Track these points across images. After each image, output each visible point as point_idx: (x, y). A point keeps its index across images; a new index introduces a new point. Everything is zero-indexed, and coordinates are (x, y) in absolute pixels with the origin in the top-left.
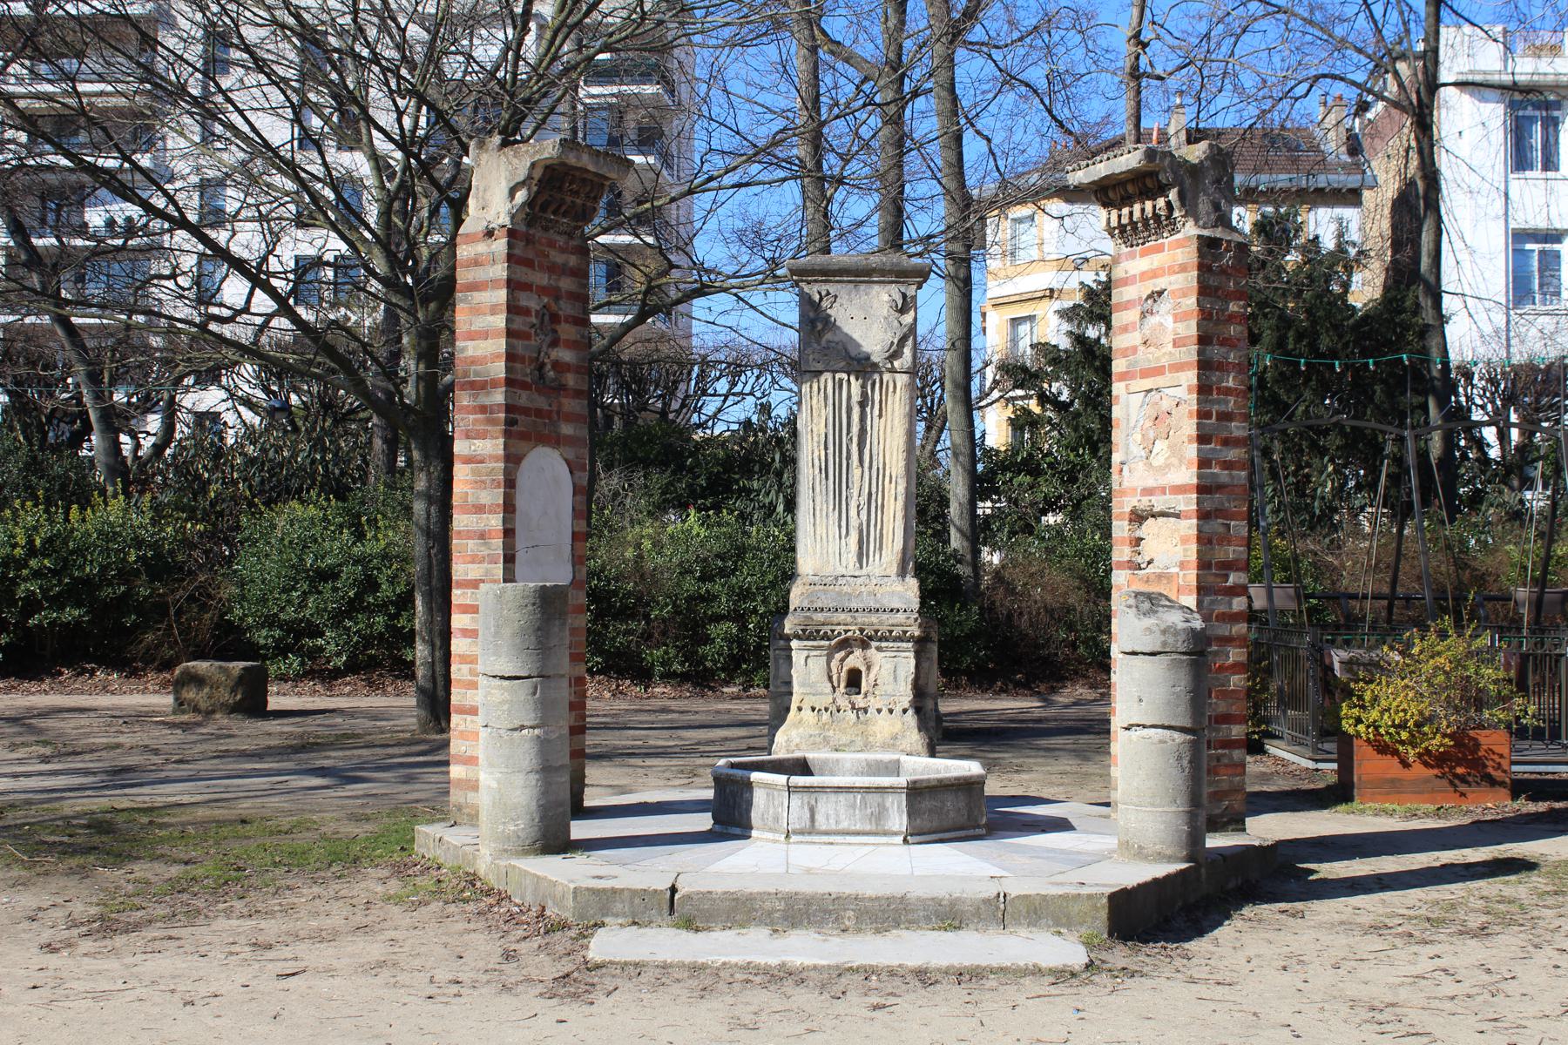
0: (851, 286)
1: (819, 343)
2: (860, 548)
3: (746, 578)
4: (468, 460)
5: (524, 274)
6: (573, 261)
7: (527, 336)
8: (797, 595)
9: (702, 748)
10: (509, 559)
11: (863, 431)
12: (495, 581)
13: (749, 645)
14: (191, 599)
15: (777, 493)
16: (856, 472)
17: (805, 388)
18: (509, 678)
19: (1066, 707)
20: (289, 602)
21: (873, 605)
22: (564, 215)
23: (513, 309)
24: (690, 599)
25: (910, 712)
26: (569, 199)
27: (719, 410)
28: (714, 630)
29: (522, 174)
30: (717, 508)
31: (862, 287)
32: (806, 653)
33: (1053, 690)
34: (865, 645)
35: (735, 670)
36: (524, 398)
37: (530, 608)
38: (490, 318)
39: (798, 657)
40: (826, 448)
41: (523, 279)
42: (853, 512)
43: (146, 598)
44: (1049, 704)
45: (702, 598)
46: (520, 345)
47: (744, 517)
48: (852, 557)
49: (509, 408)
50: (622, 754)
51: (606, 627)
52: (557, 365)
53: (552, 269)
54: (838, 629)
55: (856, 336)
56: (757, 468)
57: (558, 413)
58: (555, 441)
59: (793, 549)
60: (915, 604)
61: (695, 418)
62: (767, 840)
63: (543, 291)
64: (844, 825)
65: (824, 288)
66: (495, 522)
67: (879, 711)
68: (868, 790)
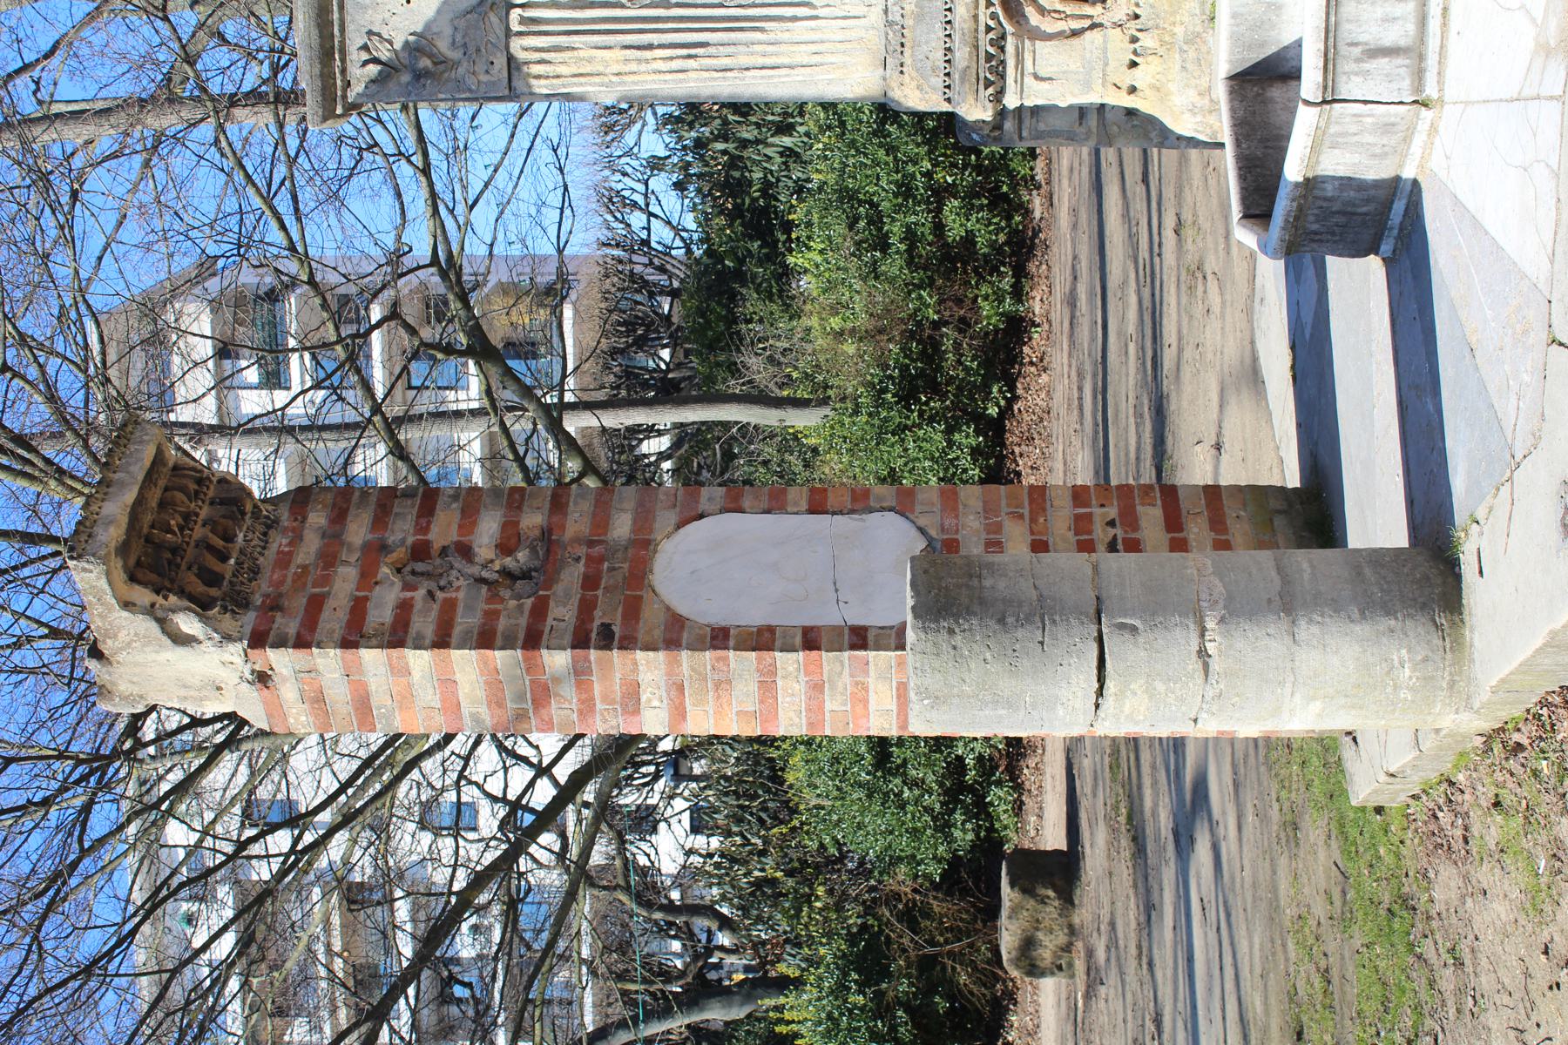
1: (455, 65)
3: (883, 189)
4: (679, 713)
5: (334, 617)
6: (317, 518)
7: (449, 607)
8: (919, 96)
9: (1144, 253)
10: (860, 638)
12: (901, 664)
13: (975, 183)
14: (914, 928)
15: (767, 145)
17: (541, 87)
18: (1101, 679)
20: (917, 802)
22: (229, 538)
23: (397, 637)
24: (910, 263)
26: (199, 532)
27: (669, 223)
28: (955, 229)
29: (148, 626)
30: (788, 227)
32: (1029, 80)
36: (563, 613)
37: (958, 639)
38: (416, 676)
40: (650, 47)
41: (343, 615)
43: (911, 984)
45: (910, 250)
46: (466, 621)
47: (799, 189)
49: (580, 641)
50: (1155, 377)
52: (505, 547)
53: (329, 559)
54: (984, 18)
56: (737, 174)
57: (591, 544)
58: (643, 546)
61: (679, 253)
63: (368, 577)
65: (356, 56)
66: (789, 663)
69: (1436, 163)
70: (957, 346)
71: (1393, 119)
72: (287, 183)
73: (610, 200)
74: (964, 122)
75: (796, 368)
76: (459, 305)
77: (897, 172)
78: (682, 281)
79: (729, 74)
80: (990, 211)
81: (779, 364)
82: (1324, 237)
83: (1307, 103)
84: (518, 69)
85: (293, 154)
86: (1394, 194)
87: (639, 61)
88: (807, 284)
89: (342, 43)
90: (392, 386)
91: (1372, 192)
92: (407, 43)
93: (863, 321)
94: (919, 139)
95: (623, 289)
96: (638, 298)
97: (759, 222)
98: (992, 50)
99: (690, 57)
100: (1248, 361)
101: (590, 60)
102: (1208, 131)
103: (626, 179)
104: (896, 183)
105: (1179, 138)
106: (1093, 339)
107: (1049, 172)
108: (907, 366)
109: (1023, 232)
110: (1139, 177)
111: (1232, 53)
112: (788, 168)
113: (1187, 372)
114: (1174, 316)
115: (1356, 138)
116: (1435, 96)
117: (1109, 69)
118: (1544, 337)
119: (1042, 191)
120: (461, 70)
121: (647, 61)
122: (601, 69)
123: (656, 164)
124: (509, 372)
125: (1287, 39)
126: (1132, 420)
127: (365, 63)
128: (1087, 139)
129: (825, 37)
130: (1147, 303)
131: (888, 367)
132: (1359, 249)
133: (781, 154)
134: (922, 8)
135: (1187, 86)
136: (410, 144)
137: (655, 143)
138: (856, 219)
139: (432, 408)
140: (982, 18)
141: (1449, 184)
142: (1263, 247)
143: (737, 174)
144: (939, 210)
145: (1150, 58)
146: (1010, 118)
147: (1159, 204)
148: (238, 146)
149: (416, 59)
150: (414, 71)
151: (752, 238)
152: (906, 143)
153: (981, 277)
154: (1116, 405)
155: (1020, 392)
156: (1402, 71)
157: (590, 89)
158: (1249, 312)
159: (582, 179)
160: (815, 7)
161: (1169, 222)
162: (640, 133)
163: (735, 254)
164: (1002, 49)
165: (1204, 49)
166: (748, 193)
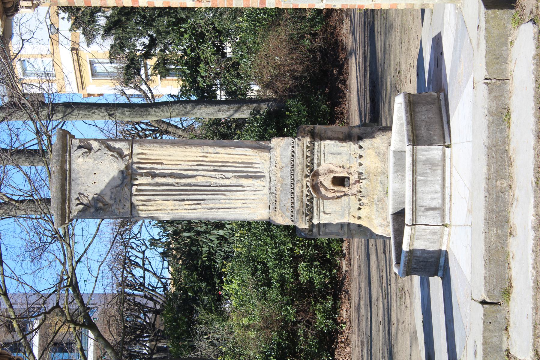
0: (72, 183)
1: (112, 205)
2: (251, 177)
3: (268, 255)
8: (283, 220)
9: (385, 285)
11: (171, 175)
15: (211, 234)
17: (143, 214)
19: (355, 40)
21: (289, 169)
24: (283, 293)
25: (361, 143)
27: (155, 274)
30: (221, 275)
31: (73, 176)
32: (322, 214)
33: (344, 49)
34: (316, 174)
35: (331, 263)
40: (184, 200)
42: (227, 182)
45: (282, 286)
54: (305, 192)
55: (107, 180)
56: (194, 249)
59: (249, 223)
61: (160, 291)
62: (448, 239)
64: (438, 187)
65: (74, 202)
67: (361, 165)
68: (414, 172)
70: (305, 335)
74: (299, 229)
77: (276, 248)
79: (212, 210)
82: (419, 270)
83: (407, 225)
84: (135, 208)
86: (440, 255)
87: (179, 205)
92: (93, 198)
97: (206, 273)
98: (308, 203)
99: (198, 204)
101: (161, 205)
102: (387, 233)
105: (377, 235)
107: (349, 249)
110: (382, 251)
111: (393, 205)
113: (400, 333)
114: (395, 310)
116: (449, 223)
117: (351, 210)
118: (470, 298)
120: (113, 208)
121: (182, 205)
122: (165, 208)
127: (77, 205)
129: (247, 198)
130: (386, 307)
132: (435, 274)
133: (218, 239)
135: (379, 217)
138: (256, 270)
140: (304, 192)
143: (194, 249)
145: (365, 207)
146: (315, 227)
149: (97, 203)
150: (96, 207)
151: (202, 281)
156: (437, 215)
162: (141, 226)
163: (193, 289)
164: (312, 203)
165: (384, 204)
166: (201, 258)
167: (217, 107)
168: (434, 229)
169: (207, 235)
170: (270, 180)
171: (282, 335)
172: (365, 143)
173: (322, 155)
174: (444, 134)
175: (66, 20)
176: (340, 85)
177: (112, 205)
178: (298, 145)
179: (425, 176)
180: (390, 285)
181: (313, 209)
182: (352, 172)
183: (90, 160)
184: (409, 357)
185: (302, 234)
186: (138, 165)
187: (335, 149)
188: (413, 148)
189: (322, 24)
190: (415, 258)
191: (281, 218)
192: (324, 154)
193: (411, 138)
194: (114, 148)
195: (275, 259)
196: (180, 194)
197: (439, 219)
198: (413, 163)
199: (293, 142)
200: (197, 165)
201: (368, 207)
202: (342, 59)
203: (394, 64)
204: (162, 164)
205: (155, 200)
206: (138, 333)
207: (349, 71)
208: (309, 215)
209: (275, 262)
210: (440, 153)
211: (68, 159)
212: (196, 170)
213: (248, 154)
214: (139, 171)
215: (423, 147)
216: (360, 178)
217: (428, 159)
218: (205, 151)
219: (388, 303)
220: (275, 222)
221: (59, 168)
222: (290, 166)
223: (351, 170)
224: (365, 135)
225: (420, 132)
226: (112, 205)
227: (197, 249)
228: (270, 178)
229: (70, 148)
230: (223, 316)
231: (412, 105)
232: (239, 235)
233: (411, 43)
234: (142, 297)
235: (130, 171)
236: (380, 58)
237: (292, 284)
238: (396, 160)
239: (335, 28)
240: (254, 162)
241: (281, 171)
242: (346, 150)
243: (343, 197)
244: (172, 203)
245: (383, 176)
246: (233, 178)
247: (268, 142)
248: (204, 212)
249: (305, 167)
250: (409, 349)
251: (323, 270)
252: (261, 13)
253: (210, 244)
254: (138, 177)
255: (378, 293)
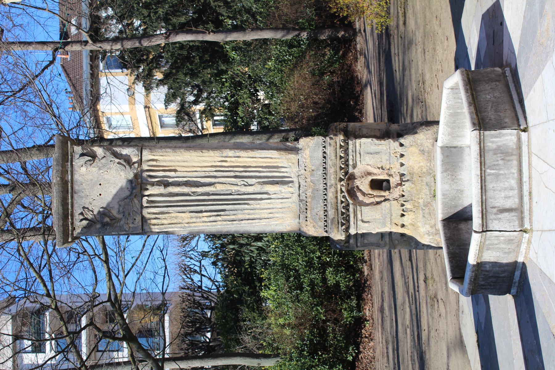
0: (75, 196)
1: (120, 220)
2: (277, 183)
3: (300, 263)
8: (314, 230)
11: (187, 184)
13: (339, 261)
16: (219, 188)
17: (155, 229)
19: (370, 72)
21: (321, 172)
25: (402, 140)
27: (210, 279)
28: (331, 280)
31: (76, 187)
32: (359, 223)
33: (359, 83)
34: (351, 178)
35: (354, 268)
39: (363, 229)
40: (201, 212)
42: (250, 189)
44: (369, 82)
45: (313, 289)
47: (265, 264)
48: (284, 190)
50: (419, 344)
51: (331, 345)
55: (114, 191)
56: (238, 258)
59: (282, 235)
60: (319, 139)
61: (214, 291)
62: (528, 248)
64: (513, 183)
65: (78, 217)
67: (402, 165)
68: (482, 164)
69: (532, 255)
70: (334, 330)
71: (512, 238)
72: (47, 265)
73: (185, 269)
75: (265, 341)
76: (119, 318)
77: (306, 257)
78: (215, 303)
79: (234, 222)
80: (346, 272)
81: (258, 339)
83: (476, 232)
84: (146, 221)
85: (50, 253)
86: (515, 269)
87: (197, 217)
88: (270, 304)
89: (72, 212)
90: (90, 354)
91: (506, 268)
92: (99, 212)
93: (293, 320)
94: (315, 243)
95: (191, 307)
96: (197, 310)
98: (344, 211)
99: (218, 215)
100: (458, 337)
102: (436, 242)
103: (192, 261)
104: (306, 261)
105: (424, 245)
106: (392, 327)
107: (370, 256)
108: (313, 340)
109: (360, 281)
110: (408, 258)
111: (443, 210)
112: (260, 255)
114: (426, 317)
115: (497, 246)
116: (529, 228)
117: (392, 217)
119: (367, 264)
120: (122, 222)
121: (200, 218)
122: (181, 221)
123: (204, 255)
124: (140, 347)
125: (466, 204)
126: (410, 362)
127: (82, 220)
128: (385, 246)
129: (274, 206)
130: (414, 311)
131: (304, 340)
133: (257, 250)
134: (314, 194)
135: (426, 224)
136: (100, 251)
137: (204, 246)
138: (289, 277)
139: (107, 361)
140: (339, 198)
141: (538, 264)
142: (461, 291)
143: (238, 258)
144: (324, 273)
145: (409, 213)
147: (417, 270)
148: (27, 250)
149: (103, 218)
151: (245, 285)
152: (310, 245)
153: (342, 300)
154: (403, 356)
155: (361, 349)
156: (515, 218)
157: (176, 229)
158: (457, 316)
159: (173, 260)
160: (269, 194)
161: (422, 277)
162: (198, 241)
163: (238, 292)
164: (348, 210)
165: (432, 208)
166: (244, 266)
167: (251, 137)
168: (510, 236)
169: (248, 247)
170: (300, 186)
171: (314, 332)
172: (407, 140)
173: (358, 155)
174: (517, 116)
175: (129, 75)
176: (356, 114)
177: (121, 219)
178: (330, 144)
179: (496, 169)
180: (418, 291)
181: (349, 218)
182: (393, 173)
183: (94, 169)
184: (445, 367)
185: (338, 246)
186: (148, 173)
187: (372, 147)
188: (480, 133)
189: (339, 62)
190: (484, 273)
191: (313, 229)
192: (360, 154)
193: (476, 122)
194: (121, 154)
195: (306, 266)
196: (196, 205)
197: (517, 223)
198: (480, 153)
199: (324, 142)
200: (216, 171)
201: (412, 213)
202: (357, 92)
203: (416, 77)
204: (175, 171)
205: (169, 213)
206: (197, 326)
207: (364, 102)
208: (344, 224)
209: (305, 269)
210: (514, 139)
211: (69, 169)
212: (215, 177)
213: (273, 157)
214: (150, 180)
215: (493, 132)
216: (402, 181)
217: (499, 147)
218: (224, 155)
219: (416, 308)
220: (305, 233)
221: (59, 179)
222: (322, 168)
223: (392, 172)
224: (405, 132)
225: (486, 114)
226: (121, 219)
227: (241, 258)
228: (299, 183)
229: (72, 156)
230: (262, 314)
231: (472, 84)
232: (274, 246)
233: (438, 48)
234: (200, 297)
235: (139, 180)
236: (398, 78)
237: (320, 287)
238: (444, 157)
239: (350, 66)
240: (280, 165)
241: (311, 175)
242: (385, 148)
243: (383, 203)
244: (188, 215)
245: (428, 177)
246: (257, 185)
247: (296, 143)
248: (224, 225)
249: (338, 169)
250: (446, 358)
251: (348, 275)
252: (287, 55)
253: (251, 254)
254: (148, 187)
255: (404, 298)
